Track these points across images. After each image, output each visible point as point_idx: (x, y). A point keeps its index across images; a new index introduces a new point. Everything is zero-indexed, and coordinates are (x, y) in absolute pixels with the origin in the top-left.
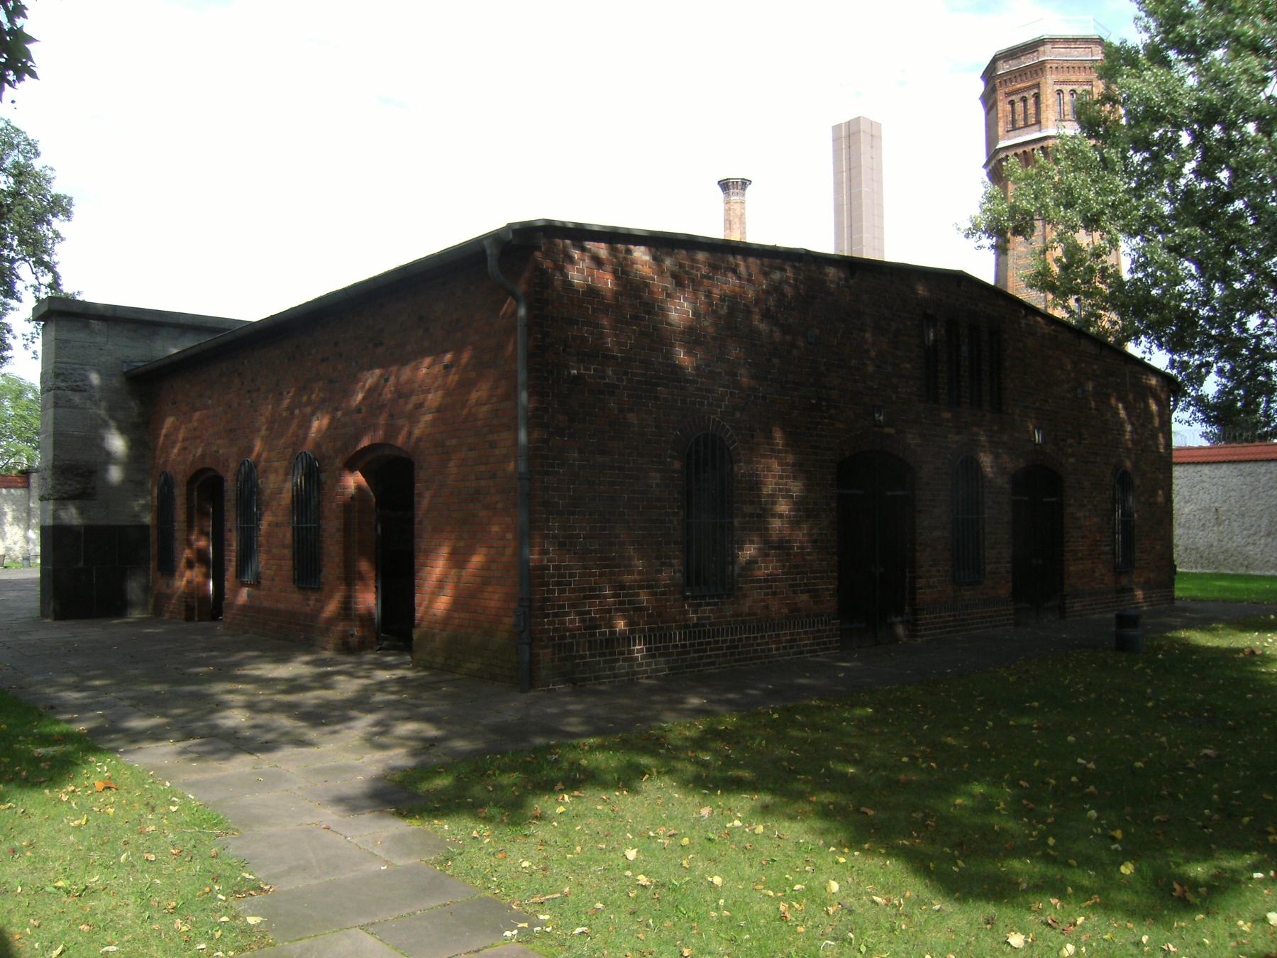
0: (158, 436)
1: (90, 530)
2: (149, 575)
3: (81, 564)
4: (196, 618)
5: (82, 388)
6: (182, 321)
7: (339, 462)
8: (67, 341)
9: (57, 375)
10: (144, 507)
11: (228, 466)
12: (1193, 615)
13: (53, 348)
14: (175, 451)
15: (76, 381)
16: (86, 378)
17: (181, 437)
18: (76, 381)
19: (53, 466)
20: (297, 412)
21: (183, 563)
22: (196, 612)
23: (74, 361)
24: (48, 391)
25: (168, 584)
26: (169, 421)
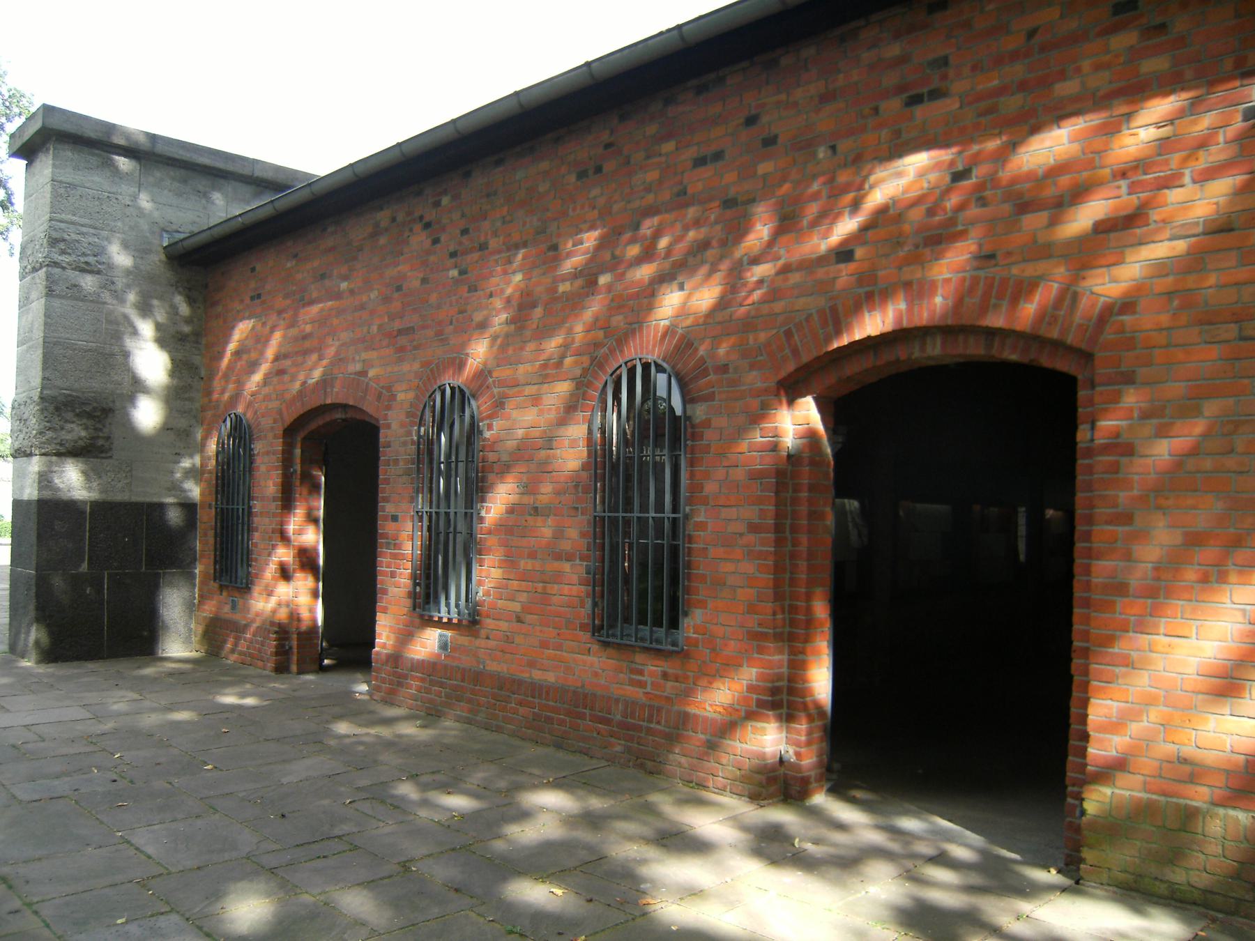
0: (220, 355)
1: (101, 509)
2: (195, 585)
3: (84, 567)
4: (294, 668)
5: (95, 266)
6: (258, 173)
7: (754, 379)
8: (72, 186)
9: (53, 242)
10: (192, 473)
11: (393, 398)
12: (627, 549)
13: (49, 196)
14: (257, 377)
15: (84, 254)
16: (100, 252)
17: (270, 353)
18: (84, 254)
19: (41, 398)
20: (603, 280)
21: (271, 570)
22: (295, 658)
23: (83, 221)
24: (35, 270)
25: (234, 607)
26: (242, 330)
